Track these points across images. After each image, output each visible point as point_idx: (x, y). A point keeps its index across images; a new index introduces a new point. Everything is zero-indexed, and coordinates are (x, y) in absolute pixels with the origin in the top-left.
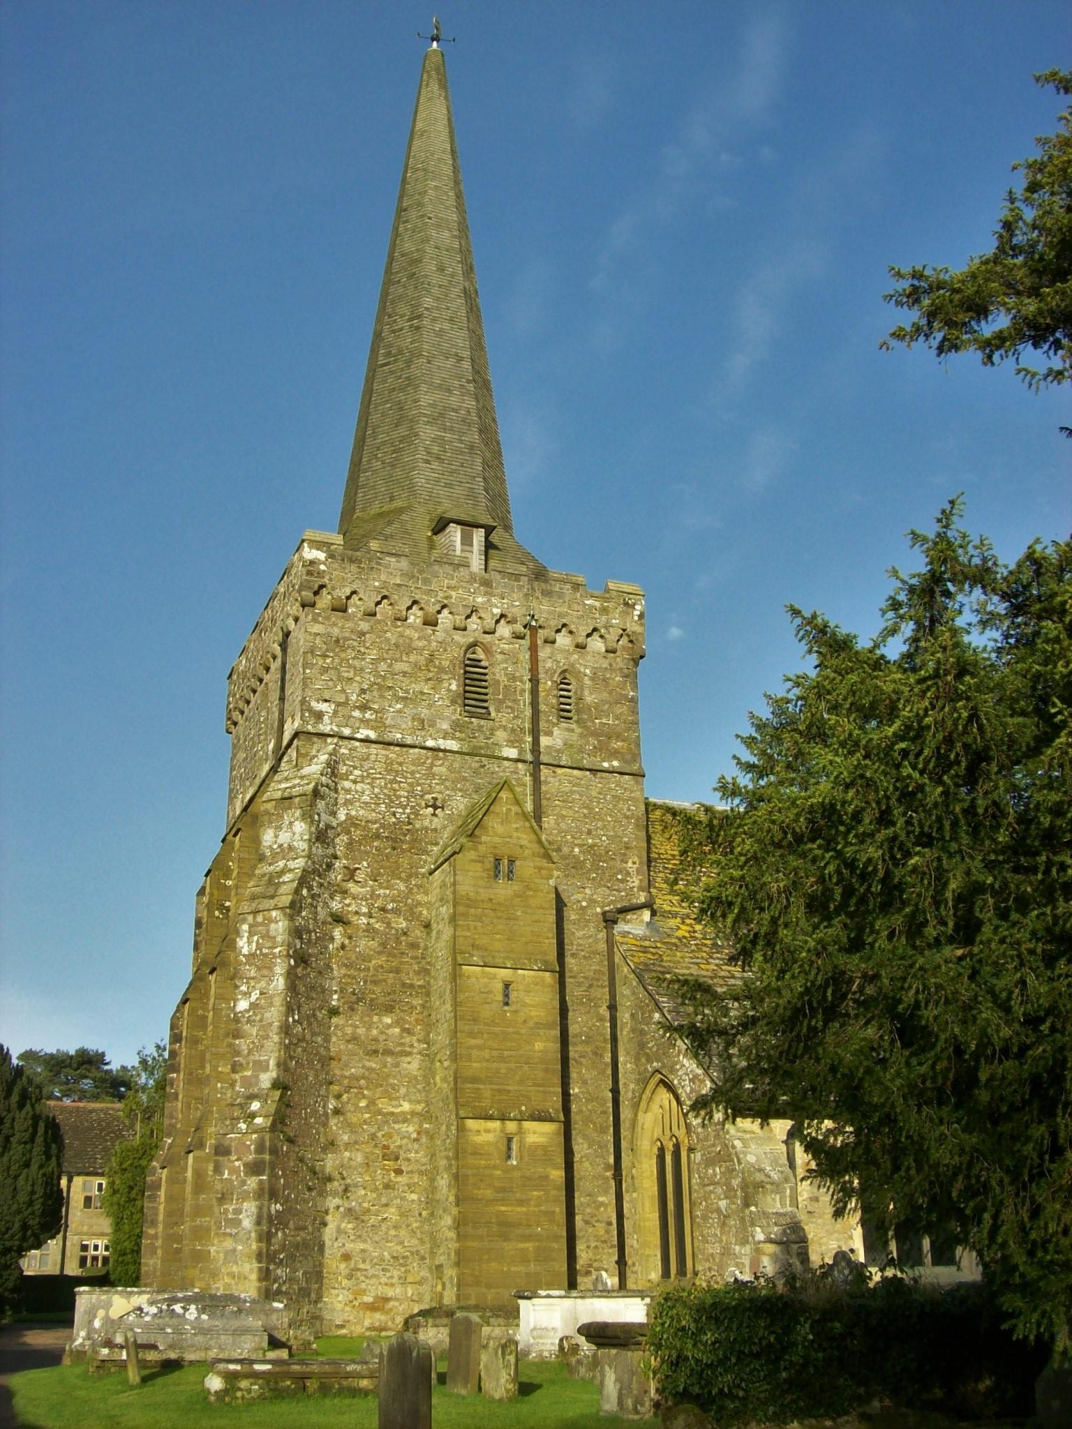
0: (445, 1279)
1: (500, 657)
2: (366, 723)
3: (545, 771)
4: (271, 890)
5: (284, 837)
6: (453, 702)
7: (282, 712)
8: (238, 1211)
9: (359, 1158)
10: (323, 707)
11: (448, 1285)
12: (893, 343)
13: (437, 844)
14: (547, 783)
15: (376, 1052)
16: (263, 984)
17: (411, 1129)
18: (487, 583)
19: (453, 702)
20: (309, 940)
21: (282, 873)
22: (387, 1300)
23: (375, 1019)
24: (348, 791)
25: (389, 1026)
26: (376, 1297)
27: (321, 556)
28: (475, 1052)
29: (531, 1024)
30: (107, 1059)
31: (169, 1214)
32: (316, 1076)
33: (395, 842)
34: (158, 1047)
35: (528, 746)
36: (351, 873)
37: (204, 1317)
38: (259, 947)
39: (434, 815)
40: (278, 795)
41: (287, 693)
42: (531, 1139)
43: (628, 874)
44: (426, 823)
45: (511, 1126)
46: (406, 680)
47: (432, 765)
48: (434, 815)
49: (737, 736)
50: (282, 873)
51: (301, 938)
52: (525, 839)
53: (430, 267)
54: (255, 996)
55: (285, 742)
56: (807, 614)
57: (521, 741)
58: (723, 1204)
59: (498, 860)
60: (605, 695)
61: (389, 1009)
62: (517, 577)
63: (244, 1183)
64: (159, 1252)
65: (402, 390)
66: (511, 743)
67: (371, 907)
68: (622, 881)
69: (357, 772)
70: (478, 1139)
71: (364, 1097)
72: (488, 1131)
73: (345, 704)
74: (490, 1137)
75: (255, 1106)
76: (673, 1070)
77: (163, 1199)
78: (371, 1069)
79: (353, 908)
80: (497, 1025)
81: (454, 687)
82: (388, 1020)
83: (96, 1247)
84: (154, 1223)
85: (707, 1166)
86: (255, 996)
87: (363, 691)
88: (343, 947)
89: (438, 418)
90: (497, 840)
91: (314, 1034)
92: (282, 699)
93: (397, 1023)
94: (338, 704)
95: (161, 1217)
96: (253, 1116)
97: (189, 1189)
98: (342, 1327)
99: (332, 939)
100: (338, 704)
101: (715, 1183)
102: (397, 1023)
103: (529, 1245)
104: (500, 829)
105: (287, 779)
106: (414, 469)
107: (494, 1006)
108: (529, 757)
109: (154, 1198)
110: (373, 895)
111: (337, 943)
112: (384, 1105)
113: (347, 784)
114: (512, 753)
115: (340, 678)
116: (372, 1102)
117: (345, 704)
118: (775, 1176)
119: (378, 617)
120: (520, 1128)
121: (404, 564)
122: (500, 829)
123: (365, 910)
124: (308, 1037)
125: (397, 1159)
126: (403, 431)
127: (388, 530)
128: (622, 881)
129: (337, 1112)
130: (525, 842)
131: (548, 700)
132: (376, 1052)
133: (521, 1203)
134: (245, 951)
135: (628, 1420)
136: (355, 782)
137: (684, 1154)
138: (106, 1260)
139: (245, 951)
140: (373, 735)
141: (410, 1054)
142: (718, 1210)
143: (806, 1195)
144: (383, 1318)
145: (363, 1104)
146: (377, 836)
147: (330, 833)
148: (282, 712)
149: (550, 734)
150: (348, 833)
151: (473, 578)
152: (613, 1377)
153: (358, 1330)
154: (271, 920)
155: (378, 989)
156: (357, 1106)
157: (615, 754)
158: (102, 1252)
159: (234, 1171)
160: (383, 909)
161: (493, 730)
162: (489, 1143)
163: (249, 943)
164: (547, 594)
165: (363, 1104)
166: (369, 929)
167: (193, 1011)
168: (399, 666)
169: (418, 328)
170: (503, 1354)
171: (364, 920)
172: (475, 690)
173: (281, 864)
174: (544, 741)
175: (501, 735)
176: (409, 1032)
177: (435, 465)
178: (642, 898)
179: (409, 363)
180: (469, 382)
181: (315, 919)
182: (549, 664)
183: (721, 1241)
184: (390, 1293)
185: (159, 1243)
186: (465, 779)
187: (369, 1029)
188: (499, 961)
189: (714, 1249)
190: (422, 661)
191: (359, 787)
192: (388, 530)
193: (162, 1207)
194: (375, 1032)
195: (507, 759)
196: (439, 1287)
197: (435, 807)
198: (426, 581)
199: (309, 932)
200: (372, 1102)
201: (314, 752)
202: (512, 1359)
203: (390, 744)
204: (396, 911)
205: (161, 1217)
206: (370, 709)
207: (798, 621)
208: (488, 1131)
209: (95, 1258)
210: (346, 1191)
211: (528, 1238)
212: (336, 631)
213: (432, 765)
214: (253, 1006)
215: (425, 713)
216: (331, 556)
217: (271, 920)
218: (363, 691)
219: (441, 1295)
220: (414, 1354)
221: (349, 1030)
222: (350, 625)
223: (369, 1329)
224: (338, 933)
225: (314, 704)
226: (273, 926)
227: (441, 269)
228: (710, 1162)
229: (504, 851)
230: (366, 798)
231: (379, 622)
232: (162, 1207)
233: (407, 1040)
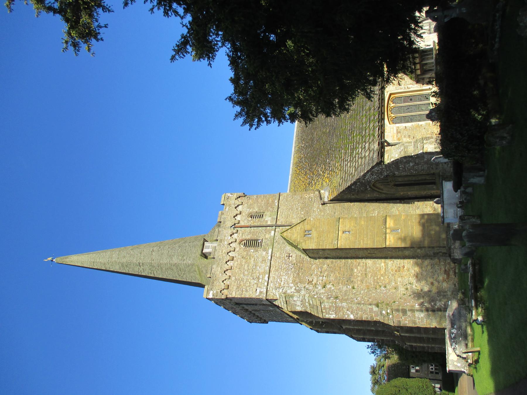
0: (438, 251)
1: (243, 237)
3: (279, 223)
4: (315, 307)
5: (299, 303)
6: (257, 251)
7: (260, 305)
8: (419, 318)
9: (399, 279)
10: (258, 291)
11: (440, 251)
12: (92, 51)
13: (301, 256)
14: (282, 222)
15: (366, 274)
16: (345, 310)
17: (390, 263)
18: (221, 241)
19: (257, 251)
20: (331, 295)
21: (310, 304)
22: (445, 270)
23: (355, 274)
24: (284, 283)
25: (357, 270)
26: (445, 274)
27: (211, 292)
28: (365, 242)
29: (356, 225)
30: (373, 365)
31: (421, 342)
32: (374, 293)
33: (300, 268)
34: (368, 348)
35: (271, 228)
36: (310, 282)
37: (455, 327)
38: (333, 311)
39: (292, 256)
40: (285, 305)
41: (254, 303)
42: (392, 225)
44: (294, 259)
45: (388, 231)
46: (250, 265)
47: (276, 257)
48: (292, 256)
49: (250, 130)
50: (310, 304)
51: (330, 298)
52: (298, 227)
53: (124, 260)
55: (270, 304)
56: (174, 53)
57: (269, 230)
58: (411, 164)
60: (255, 205)
61: (352, 270)
62: (219, 232)
63: (409, 316)
64: (433, 346)
65: (162, 268)
66: (270, 233)
67: (320, 276)
69: (278, 280)
70: (392, 241)
71: (380, 278)
72: (390, 238)
73: (257, 284)
74: (392, 238)
75: (384, 312)
76: (370, 182)
77: (416, 344)
79: (321, 282)
80: (356, 236)
81: (252, 251)
82: (356, 270)
83: (432, 369)
84: (423, 347)
85: (400, 170)
87: (253, 279)
88: (333, 285)
89: (171, 257)
90: (299, 236)
91: (360, 293)
92: (256, 305)
93: (357, 268)
95: (422, 345)
96: (388, 313)
97: (412, 335)
98: (455, 285)
99: (330, 288)
100: (257, 286)
101: (405, 166)
102: (357, 268)
104: (295, 235)
105: (281, 303)
106: (186, 264)
107: (350, 237)
108: (274, 227)
109: (416, 347)
110: (317, 275)
111: (332, 286)
112: (382, 272)
113: (282, 283)
114: (273, 232)
115: (249, 286)
116: (382, 275)
117: (257, 284)
118: (402, 148)
119: (230, 275)
120: (388, 228)
121: (214, 266)
122: (295, 235)
123: (321, 278)
124: (361, 295)
125: (399, 267)
126: (174, 268)
127: (204, 272)
129: (385, 287)
130: (300, 228)
131: (256, 222)
132: (366, 274)
133: (412, 228)
134: (334, 316)
136: (281, 281)
137: (397, 183)
138: (435, 366)
139: (334, 316)
140: (267, 276)
141: (366, 263)
142: (413, 166)
143: (408, 139)
144: (451, 272)
145: (382, 278)
146: (298, 274)
147: (297, 288)
148: (260, 305)
149: (267, 221)
150: (297, 283)
151: (219, 245)
152: (472, 179)
153: (456, 279)
154: (325, 307)
155: (346, 274)
156: (383, 280)
157: (273, 202)
158: (433, 367)
160: (321, 272)
161: (266, 239)
162: (394, 238)
163: (332, 314)
164: (224, 222)
165: (382, 278)
166: (327, 276)
167: (355, 334)
168: (246, 268)
169: (143, 264)
170: (465, 220)
172: (252, 243)
173: (307, 304)
174: (269, 223)
175: (267, 236)
177: (185, 258)
178: (317, 193)
179: (153, 267)
180: (160, 248)
181: (325, 293)
182: (246, 222)
183: (423, 165)
184: (443, 269)
185: (430, 345)
188: (337, 235)
189: (426, 167)
190: (244, 261)
191: (283, 280)
192: (204, 272)
193: (418, 345)
194: (359, 274)
195: (274, 234)
196: (441, 254)
197: (289, 256)
198: (220, 259)
199: (328, 295)
200: (382, 275)
201: (272, 294)
202: (466, 217)
204: (322, 268)
205: (422, 345)
206: (259, 276)
207: (177, 57)
208: (390, 238)
209: (436, 369)
210: (410, 284)
212: (235, 288)
213: (276, 257)
215: (260, 260)
216: (211, 289)
217: (325, 307)
218: (253, 279)
219: (444, 253)
220: (471, 230)
221: (359, 283)
222: (233, 283)
223: (455, 276)
224: (328, 286)
225: (257, 294)
226: (326, 307)
227: (124, 257)
228: (398, 169)
231: (232, 274)
232: (418, 345)
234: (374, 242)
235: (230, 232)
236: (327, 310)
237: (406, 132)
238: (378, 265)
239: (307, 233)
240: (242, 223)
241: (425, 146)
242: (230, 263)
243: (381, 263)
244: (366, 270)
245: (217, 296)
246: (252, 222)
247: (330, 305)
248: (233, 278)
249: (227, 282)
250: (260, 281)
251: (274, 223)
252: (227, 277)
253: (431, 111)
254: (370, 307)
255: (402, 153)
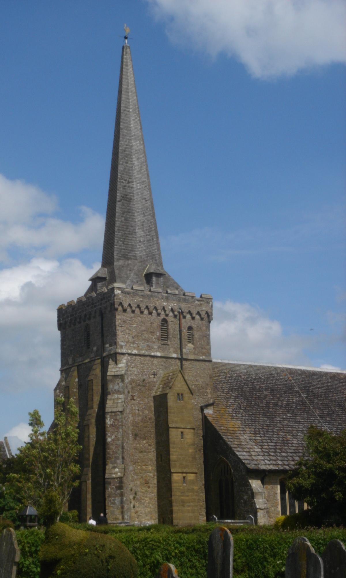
2: (135, 348)
3: (184, 362)
5: (116, 387)
25: (145, 444)
27: (120, 292)
39: (154, 377)
43: (207, 393)
48: (154, 377)
54: (113, 437)
59: (178, 394)
61: (145, 439)
66: (175, 352)
68: (206, 396)
69: (133, 364)
74: (179, 478)
78: (140, 457)
86: (113, 437)
94: (127, 342)
102: (147, 443)
103: (189, 508)
114: (175, 356)
128: (206, 396)
133: (187, 496)
134: (109, 423)
135: (57, 517)
136: (132, 368)
159: (112, 489)
163: (110, 421)
166: (139, 415)
171: (137, 411)
174: (184, 351)
176: (150, 445)
186: (162, 365)
187: (140, 444)
191: (134, 369)
197: (154, 375)
203: (103, 336)
211: (189, 506)
214: (113, 440)
216: (122, 292)
222: (128, 315)
229: (180, 392)
230: (135, 373)
233: (150, 447)
234: (175, 461)
235: (176, 308)
236: (114, 418)
237: (272, 493)
238: (149, 463)
239: (180, 396)
240: (183, 320)
241: (262, 511)
242: (146, 312)
243: (152, 466)
244: (145, 452)
245: (117, 299)
246: (185, 331)
247: (120, 420)
248: (132, 315)
249: (129, 310)
250: (132, 345)
251: (184, 357)
252: (134, 308)
253: (69, 505)
254: (120, 457)
255: (256, 491)
